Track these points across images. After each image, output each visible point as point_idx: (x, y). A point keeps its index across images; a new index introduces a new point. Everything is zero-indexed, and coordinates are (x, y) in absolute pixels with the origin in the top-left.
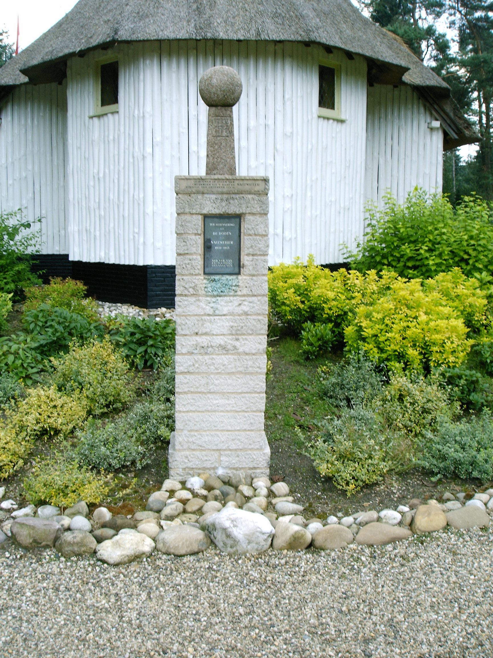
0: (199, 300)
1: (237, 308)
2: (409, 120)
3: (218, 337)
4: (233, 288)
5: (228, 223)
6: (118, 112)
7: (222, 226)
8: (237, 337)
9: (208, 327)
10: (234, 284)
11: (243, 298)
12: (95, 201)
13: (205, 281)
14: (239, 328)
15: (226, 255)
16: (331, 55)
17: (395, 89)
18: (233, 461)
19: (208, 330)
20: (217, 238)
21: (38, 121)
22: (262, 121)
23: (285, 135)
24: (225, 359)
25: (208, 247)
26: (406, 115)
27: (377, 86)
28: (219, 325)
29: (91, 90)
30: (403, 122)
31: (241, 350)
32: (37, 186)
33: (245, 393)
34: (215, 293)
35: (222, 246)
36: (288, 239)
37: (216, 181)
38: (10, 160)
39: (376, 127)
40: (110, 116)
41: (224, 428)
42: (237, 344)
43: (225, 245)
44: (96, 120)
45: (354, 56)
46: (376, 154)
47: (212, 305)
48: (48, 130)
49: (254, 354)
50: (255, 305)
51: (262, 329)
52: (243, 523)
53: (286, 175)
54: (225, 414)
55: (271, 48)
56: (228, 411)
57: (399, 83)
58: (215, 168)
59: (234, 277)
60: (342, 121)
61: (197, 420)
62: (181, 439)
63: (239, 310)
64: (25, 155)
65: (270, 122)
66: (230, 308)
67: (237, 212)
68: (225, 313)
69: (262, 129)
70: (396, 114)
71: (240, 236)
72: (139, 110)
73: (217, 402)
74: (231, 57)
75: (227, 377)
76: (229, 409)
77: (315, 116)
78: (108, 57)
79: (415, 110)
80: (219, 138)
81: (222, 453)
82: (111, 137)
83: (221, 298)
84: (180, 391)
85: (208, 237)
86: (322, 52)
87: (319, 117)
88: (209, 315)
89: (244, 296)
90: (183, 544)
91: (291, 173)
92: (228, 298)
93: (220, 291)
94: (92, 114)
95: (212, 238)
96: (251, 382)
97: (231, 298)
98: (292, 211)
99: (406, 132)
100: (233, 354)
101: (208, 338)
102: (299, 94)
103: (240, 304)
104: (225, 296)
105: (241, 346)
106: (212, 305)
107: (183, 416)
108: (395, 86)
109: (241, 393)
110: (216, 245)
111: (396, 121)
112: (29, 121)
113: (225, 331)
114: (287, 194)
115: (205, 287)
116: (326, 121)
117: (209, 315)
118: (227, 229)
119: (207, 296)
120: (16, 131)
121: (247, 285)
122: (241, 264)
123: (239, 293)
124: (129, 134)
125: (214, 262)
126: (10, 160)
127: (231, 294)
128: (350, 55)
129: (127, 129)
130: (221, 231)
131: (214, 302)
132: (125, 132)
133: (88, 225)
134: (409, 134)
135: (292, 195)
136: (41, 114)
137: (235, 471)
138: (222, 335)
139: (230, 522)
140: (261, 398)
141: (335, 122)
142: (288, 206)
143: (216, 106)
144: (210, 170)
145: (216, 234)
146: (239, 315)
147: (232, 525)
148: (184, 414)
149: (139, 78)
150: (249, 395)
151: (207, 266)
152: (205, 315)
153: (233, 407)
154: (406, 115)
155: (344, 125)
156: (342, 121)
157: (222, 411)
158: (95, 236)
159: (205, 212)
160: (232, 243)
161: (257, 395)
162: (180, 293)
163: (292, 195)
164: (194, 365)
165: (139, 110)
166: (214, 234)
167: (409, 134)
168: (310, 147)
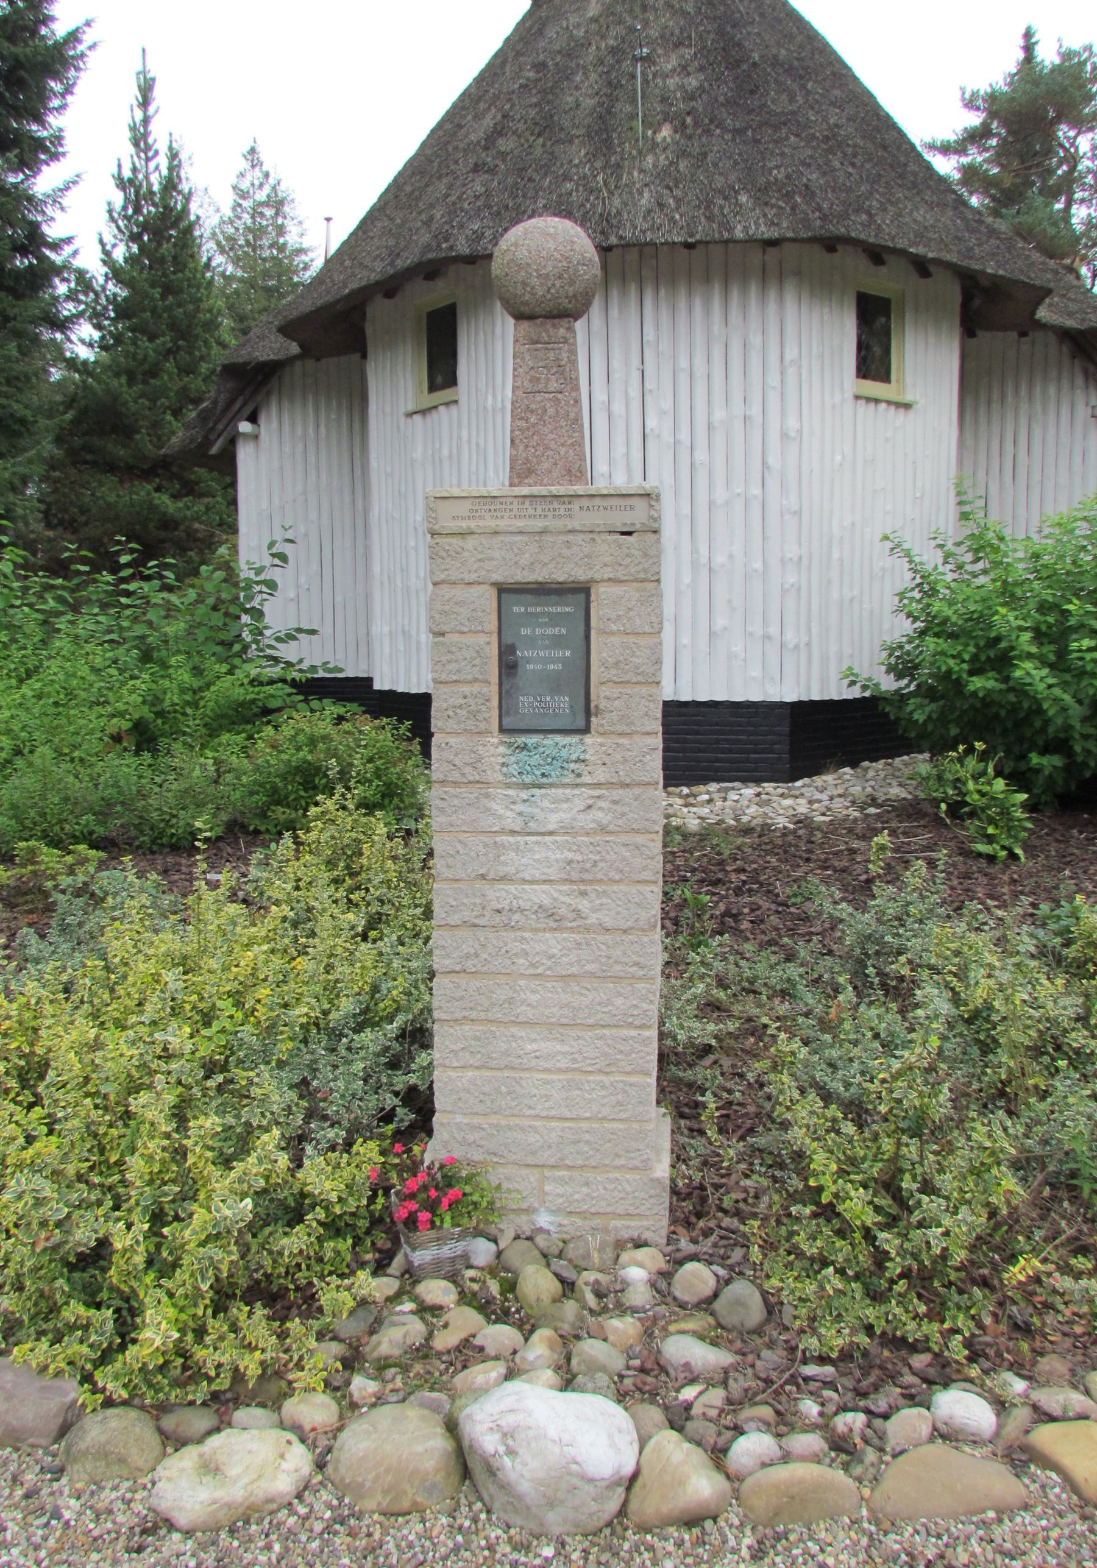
0: (487, 796)
1: (582, 816)
2: (1052, 406)
3: (536, 887)
4: (572, 766)
5: (557, 604)
6: (456, 402)
7: (543, 614)
8: (583, 888)
9: (512, 862)
10: (574, 757)
11: (597, 793)
12: (418, 577)
13: (502, 749)
14: (588, 865)
15: (556, 684)
16: (883, 270)
17: (1024, 339)
18: (577, 1196)
19: (510, 870)
20: (532, 643)
21: (328, 430)
22: (738, 409)
23: (784, 436)
24: (552, 942)
25: (508, 665)
26: (1044, 392)
27: (984, 337)
28: (537, 857)
29: (409, 362)
30: (1038, 408)
31: (593, 919)
32: (327, 551)
33: (603, 1026)
34: (528, 779)
35: (545, 661)
36: (791, 646)
37: (527, 502)
38: (276, 502)
39: (983, 420)
40: (442, 408)
41: (553, 1113)
42: (584, 904)
43: (553, 661)
44: (417, 418)
45: (932, 269)
46: (981, 474)
47: (520, 807)
48: (345, 445)
49: (625, 931)
50: (626, 809)
51: (645, 868)
52: (533, 1445)
53: (787, 517)
54: (554, 1077)
55: (756, 257)
56: (560, 1070)
57: (1028, 326)
58: (530, 472)
59: (574, 739)
60: (907, 406)
61: (486, 1089)
62: (31, 1416)
63: (586, 821)
64: (305, 492)
65: (755, 411)
66: (564, 816)
67: (582, 579)
68: (551, 827)
69: (738, 425)
70: (1023, 392)
71: (587, 637)
72: (494, 396)
73: (535, 1046)
74: (673, 283)
75: (558, 985)
76: (563, 1064)
77: (849, 395)
78: (435, 294)
79: (1065, 384)
80: (539, 397)
81: (547, 1173)
82: (445, 452)
83: (543, 791)
84: (443, 1016)
85: (508, 640)
86: (863, 262)
87: (857, 397)
88: (513, 832)
89: (597, 785)
90: (377, 1478)
91: (799, 513)
92: (560, 791)
93: (538, 773)
94: (411, 407)
95: (517, 644)
96: (619, 1001)
97: (568, 791)
98: (799, 589)
99: (1045, 429)
100: (572, 930)
101: (512, 888)
102: (815, 352)
103: (590, 807)
104: (551, 785)
105: (594, 910)
106: (520, 807)
107: (450, 1078)
108: (1023, 334)
109: (591, 1026)
110: (529, 661)
111: (1024, 406)
112: (311, 431)
113: (553, 873)
114: (789, 555)
115: (503, 764)
116: (872, 405)
117: (513, 832)
118: (555, 620)
119: (508, 786)
120: (287, 449)
121: (607, 760)
122: (592, 705)
123: (586, 779)
124: (477, 444)
125: (525, 702)
126: (276, 502)
127: (567, 780)
128: (922, 267)
129: (474, 433)
130: (541, 626)
131: (524, 801)
132: (469, 441)
133: (406, 622)
134: (1052, 430)
135: (800, 557)
136: (333, 416)
137: (579, 1222)
138: (545, 881)
139: (497, 1436)
140: (645, 1041)
141: (892, 408)
142: (792, 579)
143: (531, 317)
144: (519, 476)
145: (529, 631)
146: (587, 834)
147: (502, 1449)
148: (453, 1074)
149: (493, 331)
150: (614, 1031)
151: (508, 713)
152: (502, 832)
153: (575, 1061)
154: (1044, 392)
155: (911, 414)
156: (907, 406)
157: (547, 1070)
158: (418, 643)
159: (497, 577)
160: (568, 654)
161: (633, 1033)
162: (442, 777)
163: (800, 557)
164: (477, 955)
165: (494, 396)
166: (523, 631)
167: (1052, 430)
168: (839, 458)
